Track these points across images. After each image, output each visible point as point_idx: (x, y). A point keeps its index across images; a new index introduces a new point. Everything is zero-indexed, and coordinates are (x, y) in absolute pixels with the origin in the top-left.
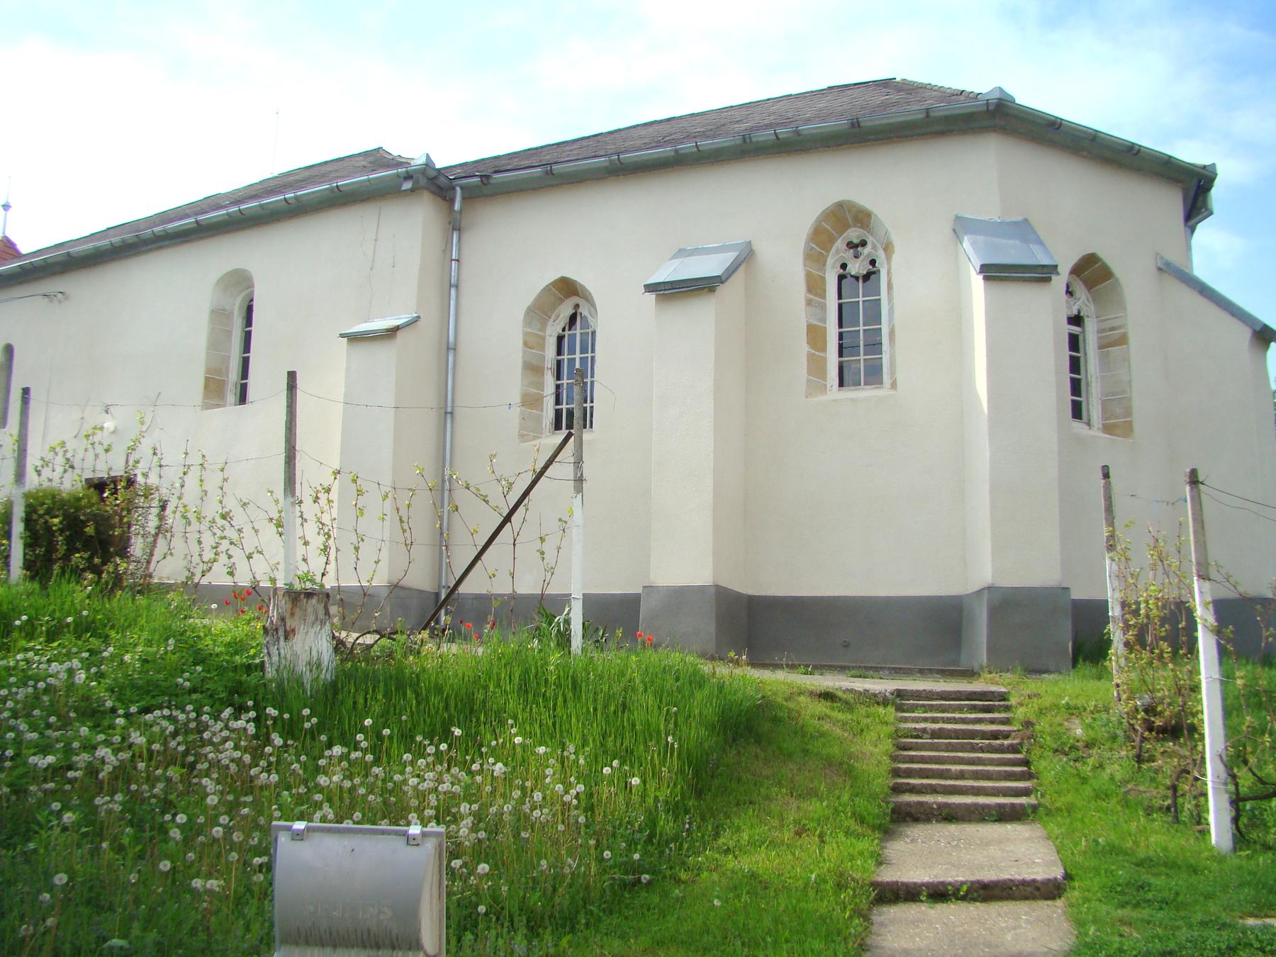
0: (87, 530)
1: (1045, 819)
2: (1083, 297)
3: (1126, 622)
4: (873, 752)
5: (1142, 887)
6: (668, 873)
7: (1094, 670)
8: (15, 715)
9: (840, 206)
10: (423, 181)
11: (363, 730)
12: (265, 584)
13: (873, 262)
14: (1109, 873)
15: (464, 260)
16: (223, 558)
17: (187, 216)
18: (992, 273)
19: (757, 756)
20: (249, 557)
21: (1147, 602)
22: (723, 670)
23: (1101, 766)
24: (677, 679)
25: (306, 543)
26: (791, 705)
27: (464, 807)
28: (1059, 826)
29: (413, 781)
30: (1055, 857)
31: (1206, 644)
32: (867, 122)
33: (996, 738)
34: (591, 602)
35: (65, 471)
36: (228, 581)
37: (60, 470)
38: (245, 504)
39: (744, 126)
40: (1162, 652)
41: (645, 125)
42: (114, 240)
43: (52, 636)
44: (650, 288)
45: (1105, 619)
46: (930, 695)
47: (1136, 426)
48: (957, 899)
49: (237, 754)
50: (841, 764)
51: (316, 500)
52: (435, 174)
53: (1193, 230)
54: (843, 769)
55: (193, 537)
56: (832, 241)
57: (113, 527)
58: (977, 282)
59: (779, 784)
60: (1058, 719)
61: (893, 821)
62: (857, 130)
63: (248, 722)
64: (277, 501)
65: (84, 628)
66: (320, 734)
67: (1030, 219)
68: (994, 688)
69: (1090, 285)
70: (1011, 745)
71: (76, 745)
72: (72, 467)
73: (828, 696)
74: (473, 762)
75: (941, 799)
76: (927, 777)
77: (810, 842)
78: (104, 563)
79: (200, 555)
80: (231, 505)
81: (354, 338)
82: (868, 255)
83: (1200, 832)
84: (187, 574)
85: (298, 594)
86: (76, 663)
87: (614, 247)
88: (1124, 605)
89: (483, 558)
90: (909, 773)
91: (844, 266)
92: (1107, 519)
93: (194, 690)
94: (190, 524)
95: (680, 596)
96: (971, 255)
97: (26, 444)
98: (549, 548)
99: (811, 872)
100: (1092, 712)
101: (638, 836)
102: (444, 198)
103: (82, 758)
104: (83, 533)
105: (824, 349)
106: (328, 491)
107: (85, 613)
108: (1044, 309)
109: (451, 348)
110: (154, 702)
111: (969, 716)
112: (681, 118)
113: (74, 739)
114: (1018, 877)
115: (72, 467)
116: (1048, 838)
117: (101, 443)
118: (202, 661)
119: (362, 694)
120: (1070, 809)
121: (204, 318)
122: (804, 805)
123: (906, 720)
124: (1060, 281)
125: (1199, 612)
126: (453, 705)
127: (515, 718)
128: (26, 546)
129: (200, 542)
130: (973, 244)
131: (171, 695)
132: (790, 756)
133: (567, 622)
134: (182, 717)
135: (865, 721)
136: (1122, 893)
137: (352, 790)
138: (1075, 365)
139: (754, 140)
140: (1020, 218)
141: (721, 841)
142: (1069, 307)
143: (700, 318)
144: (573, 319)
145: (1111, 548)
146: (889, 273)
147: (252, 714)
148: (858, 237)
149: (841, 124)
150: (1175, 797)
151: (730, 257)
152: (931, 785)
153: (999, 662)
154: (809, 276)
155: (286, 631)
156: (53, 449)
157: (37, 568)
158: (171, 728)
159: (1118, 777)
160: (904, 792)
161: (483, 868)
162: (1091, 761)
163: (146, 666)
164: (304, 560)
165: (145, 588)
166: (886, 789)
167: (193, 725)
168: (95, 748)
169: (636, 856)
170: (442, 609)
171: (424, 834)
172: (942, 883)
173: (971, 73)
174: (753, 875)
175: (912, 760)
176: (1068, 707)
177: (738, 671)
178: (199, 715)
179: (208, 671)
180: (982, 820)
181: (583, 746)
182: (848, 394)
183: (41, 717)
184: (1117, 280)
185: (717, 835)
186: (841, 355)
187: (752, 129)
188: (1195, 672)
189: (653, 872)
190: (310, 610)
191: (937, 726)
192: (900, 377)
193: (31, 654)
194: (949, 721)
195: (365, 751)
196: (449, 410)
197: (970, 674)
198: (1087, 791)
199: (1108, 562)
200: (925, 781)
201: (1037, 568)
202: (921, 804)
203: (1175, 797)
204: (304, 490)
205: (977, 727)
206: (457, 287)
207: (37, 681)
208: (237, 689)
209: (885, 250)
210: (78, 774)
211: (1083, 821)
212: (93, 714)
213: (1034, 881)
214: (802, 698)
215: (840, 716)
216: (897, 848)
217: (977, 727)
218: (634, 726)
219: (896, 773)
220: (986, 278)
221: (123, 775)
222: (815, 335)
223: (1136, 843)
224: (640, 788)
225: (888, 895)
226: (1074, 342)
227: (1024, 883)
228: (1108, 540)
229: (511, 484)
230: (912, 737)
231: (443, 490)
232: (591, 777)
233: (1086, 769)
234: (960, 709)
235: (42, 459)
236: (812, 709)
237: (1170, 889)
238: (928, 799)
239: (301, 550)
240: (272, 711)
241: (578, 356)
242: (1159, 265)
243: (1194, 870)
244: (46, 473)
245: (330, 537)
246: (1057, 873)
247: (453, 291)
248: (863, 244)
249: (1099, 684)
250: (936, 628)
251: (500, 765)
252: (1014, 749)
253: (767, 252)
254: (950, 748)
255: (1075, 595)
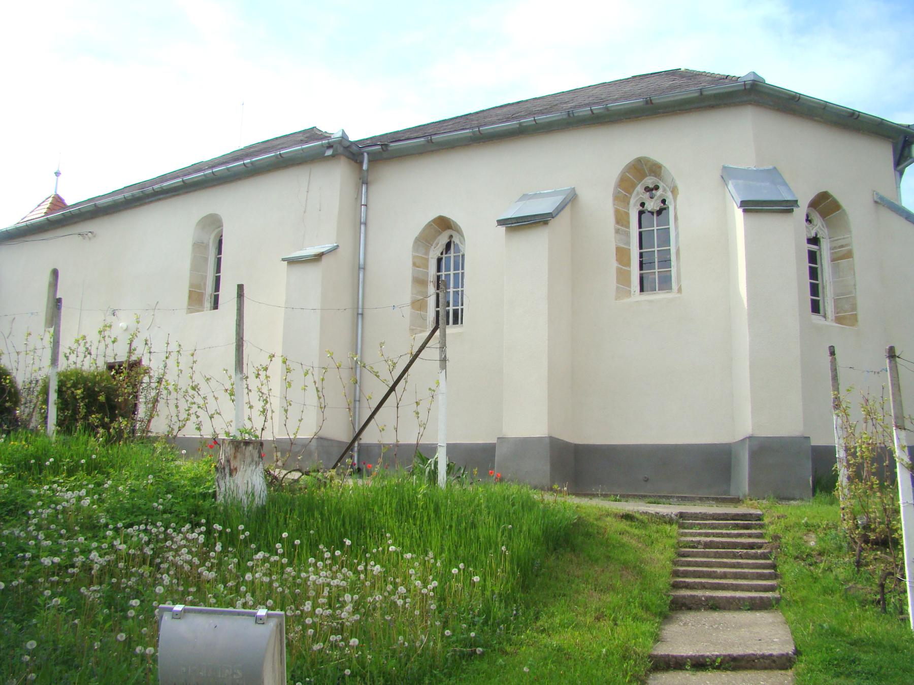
0: (100, 398)
1: (786, 608)
2: (819, 224)
3: (848, 461)
4: (660, 559)
5: (854, 661)
6: (497, 646)
7: (828, 498)
8: (39, 527)
9: (639, 161)
10: (341, 150)
11: (281, 540)
12: (222, 436)
13: (664, 201)
14: (829, 650)
15: (370, 206)
16: (193, 418)
17: (178, 177)
18: (750, 207)
19: (571, 561)
20: (211, 417)
21: (861, 446)
22: (549, 498)
23: (830, 569)
24: (513, 505)
25: (251, 407)
26: (601, 524)
27: (347, 597)
28: (796, 614)
29: (313, 577)
30: (789, 637)
31: (902, 476)
32: (656, 100)
33: (753, 548)
34: (452, 449)
35: (85, 357)
36: (196, 435)
37: (81, 355)
38: (208, 379)
39: (569, 105)
40: (872, 484)
41: (502, 107)
42: (126, 195)
43: (71, 472)
44: (501, 222)
45: (834, 460)
46: (704, 517)
47: (859, 317)
48: (714, 668)
49: (189, 557)
50: (635, 567)
51: (258, 376)
52: (348, 144)
53: (901, 173)
54: (637, 570)
55: (172, 403)
56: (634, 186)
57: (118, 396)
58: (739, 213)
59: (587, 582)
60: (799, 534)
61: (671, 609)
62: (649, 106)
63: (199, 534)
64: (230, 377)
65: (93, 467)
66: (251, 543)
67: (778, 168)
68: (752, 511)
69: (824, 215)
70: (763, 553)
71: (77, 550)
72: (90, 354)
73: (628, 517)
74: (359, 564)
75: (708, 593)
76: (699, 577)
77: (606, 625)
78: (111, 422)
79: (177, 416)
80: (198, 379)
81: (292, 262)
82: (660, 196)
83: (902, 620)
84: (168, 429)
85: (239, 442)
86: (84, 492)
87: (476, 193)
88: (847, 449)
89: (376, 417)
90: (686, 574)
91: (643, 205)
92: (833, 386)
93: (164, 512)
94: (170, 393)
95: (524, 445)
96: (733, 196)
97: (59, 338)
98: (422, 409)
99: (604, 647)
100: (825, 529)
101: (476, 619)
102: (356, 161)
103: (79, 559)
104: (103, 401)
105: (629, 265)
106: (266, 369)
107: (94, 456)
108: (789, 234)
109: (362, 268)
110: (136, 520)
111: (733, 532)
112: (527, 101)
113: (76, 546)
114: (759, 652)
115: (90, 354)
116: (786, 622)
117: (109, 337)
118: (173, 491)
119: (283, 515)
120: (804, 601)
121: (189, 247)
122: (603, 597)
123: (685, 535)
124: (801, 212)
125: (897, 453)
126: (347, 523)
127: (392, 532)
128: (59, 409)
129: (177, 407)
130: (735, 186)
131: (148, 515)
132: (597, 561)
133: (436, 463)
134: (154, 530)
135: (655, 536)
136: (837, 665)
137: (270, 583)
138: (813, 274)
139: (576, 115)
140: (771, 167)
141: (538, 624)
142: (809, 232)
143: (537, 243)
144: (448, 246)
145: (837, 406)
146: (675, 208)
147: (203, 529)
148: (653, 183)
149: (638, 102)
150: (883, 593)
151: (558, 200)
152: (701, 583)
153: (757, 492)
154: (617, 212)
155: (230, 470)
156: (77, 341)
157: (65, 425)
158: (146, 538)
159: (841, 577)
160: (681, 588)
161: (354, 641)
162: (822, 565)
163: (134, 494)
164: (250, 419)
165: (148, 440)
166: (668, 586)
167: (162, 536)
168: (90, 552)
169: (473, 634)
170: (352, 454)
171: (268, 616)
172: (702, 656)
173: (734, 64)
174: (560, 649)
175: (689, 564)
176: (807, 525)
177: (560, 499)
178: (166, 529)
179: (176, 498)
180: (739, 609)
181: (441, 554)
182: (647, 297)
183: (55, 531)
184: (844, 210)
185: (537, 618)
186: (641, 268)
187: (575, 107)
188: (895, 499)
189: (486, 645)
190: (247, 454)
191: (708, 539)
192: (684, 284)
193: (55, 486)
194: (717, 535)
195: (283, 556)
196: (360, 312)
197: (737, 501)
198: (818, 587)
199: (835, 417)
200: (698, 580)
201: (786, 422)
202: (693, 597)
203: (883, 593)
204: (249, 370)
205: (739, 540)
206: (365, 224)
207: (57, 505)
208: (196, 511)
209: (672, 192)
210: (76, 570)
211: (813, 612)
212: (92, 528)
213: (771, 655)
214: (609, 519)
215: (636, 531)
216: (672, 630)
217: (739, 540)
218: (479, 538)
219: (676, 574)
220: (744, 211)
221: (108, 571)
222: (622, 255)
223: (851, 627)
224: (481, 584)
225: (662, 665)
226: (813, 257)
227: (763, 657)
228: (834, 401)
229: (395, 364)
230: (690, 547)
231: (357, 369)
232: (444, 578)
233: (818, 572)
234: (726, 527)
235: (70, 348)
236: (615, 526)
237: (875, 664)
238: (699, 593)
239: (247, 411)
240: (218, 527)
241: (452, 272)
242: (876, 199)
243: (895, 649)
244: (73, 358)
245: (267, 402)
246: (789, 649)
247: (363, 227)
248: (657, 188)
249: (830, 508)
250: (710, 466)
251: (378, 566)
252: (765, 556)
253: (586, 196)
254: (717, 555)
255: (814, 442)
